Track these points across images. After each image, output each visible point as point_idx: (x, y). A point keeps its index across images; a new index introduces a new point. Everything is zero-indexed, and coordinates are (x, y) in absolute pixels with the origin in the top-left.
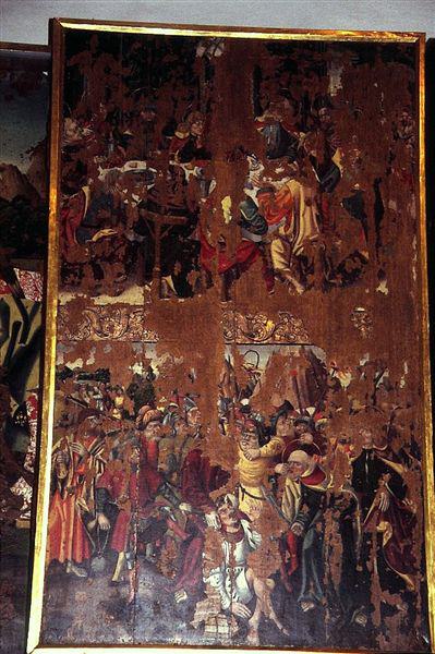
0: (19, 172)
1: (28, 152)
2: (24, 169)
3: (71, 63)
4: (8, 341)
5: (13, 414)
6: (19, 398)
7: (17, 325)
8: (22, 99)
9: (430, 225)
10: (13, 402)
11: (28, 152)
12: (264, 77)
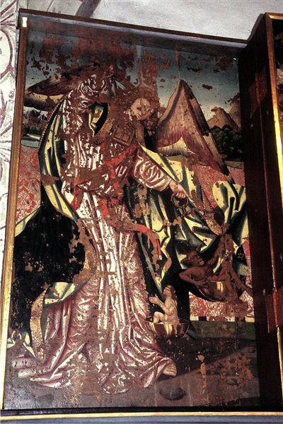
0: (225, 112)
1: (229, 101)
2: (228, 110)
3: (277, 38)
4: (229, 208)
5: (236, 252)
6: (238, 243)
7: (232, 199)
8: (224, 71)
9: (233, 50)
10: (235, 245)
11: (229, 101)
12: (48, 65)
